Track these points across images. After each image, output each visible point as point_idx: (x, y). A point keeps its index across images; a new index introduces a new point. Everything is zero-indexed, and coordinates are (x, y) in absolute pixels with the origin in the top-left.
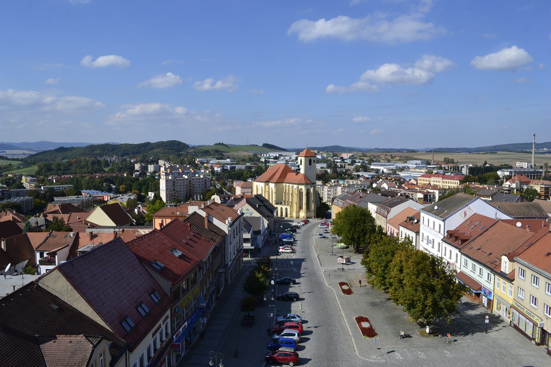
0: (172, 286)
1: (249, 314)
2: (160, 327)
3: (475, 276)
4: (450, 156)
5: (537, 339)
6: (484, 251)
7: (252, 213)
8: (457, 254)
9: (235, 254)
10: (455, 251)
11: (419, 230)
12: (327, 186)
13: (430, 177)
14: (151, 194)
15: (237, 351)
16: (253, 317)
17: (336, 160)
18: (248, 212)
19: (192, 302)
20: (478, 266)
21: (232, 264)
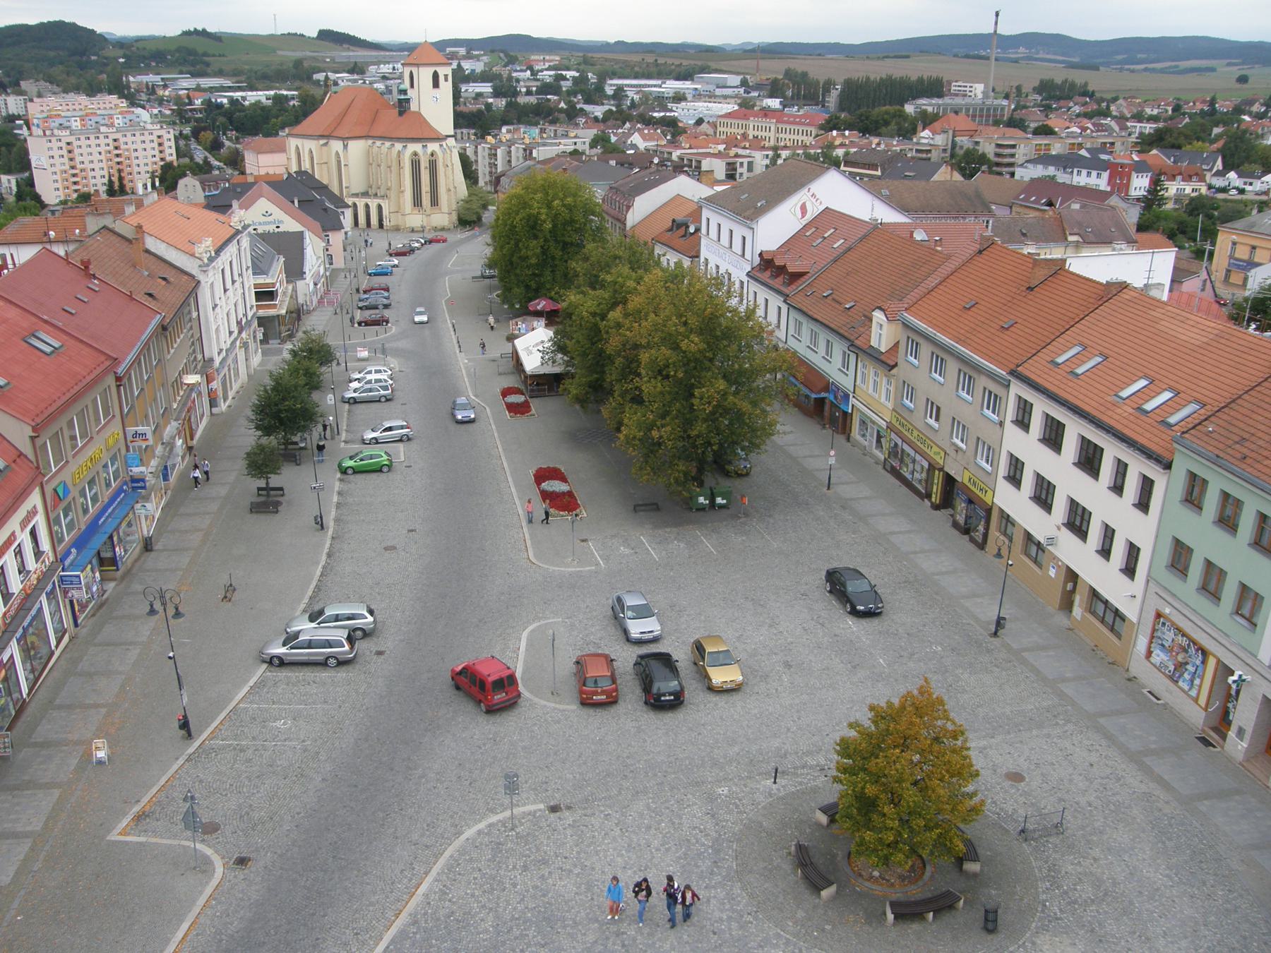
0: (34, 429)
1: (267, 483)
2: (15, 539)
3: (816, 359)
4: (799, 65)
5: (934, 496)
6: (837, 298)
7: (279, 222)
8: (780, 308)
9: (231, 333)
10: (776, 301)
11: (699, 251)
12: (486, 143)
13: (746, 117)
14: (9, 181)
15: (231, 585)
16: (281, 489)
17: (514, 74)
18: (270, 219)
19: (105, 466)
20: (823, 336)
21: (224, 360)
